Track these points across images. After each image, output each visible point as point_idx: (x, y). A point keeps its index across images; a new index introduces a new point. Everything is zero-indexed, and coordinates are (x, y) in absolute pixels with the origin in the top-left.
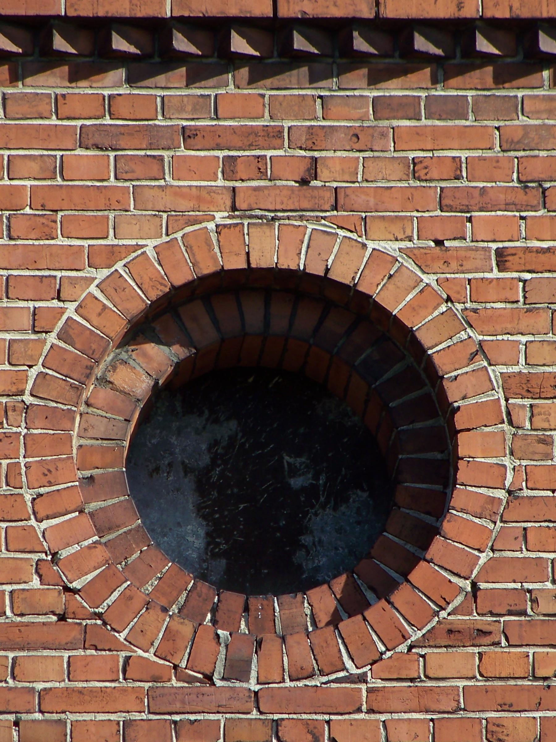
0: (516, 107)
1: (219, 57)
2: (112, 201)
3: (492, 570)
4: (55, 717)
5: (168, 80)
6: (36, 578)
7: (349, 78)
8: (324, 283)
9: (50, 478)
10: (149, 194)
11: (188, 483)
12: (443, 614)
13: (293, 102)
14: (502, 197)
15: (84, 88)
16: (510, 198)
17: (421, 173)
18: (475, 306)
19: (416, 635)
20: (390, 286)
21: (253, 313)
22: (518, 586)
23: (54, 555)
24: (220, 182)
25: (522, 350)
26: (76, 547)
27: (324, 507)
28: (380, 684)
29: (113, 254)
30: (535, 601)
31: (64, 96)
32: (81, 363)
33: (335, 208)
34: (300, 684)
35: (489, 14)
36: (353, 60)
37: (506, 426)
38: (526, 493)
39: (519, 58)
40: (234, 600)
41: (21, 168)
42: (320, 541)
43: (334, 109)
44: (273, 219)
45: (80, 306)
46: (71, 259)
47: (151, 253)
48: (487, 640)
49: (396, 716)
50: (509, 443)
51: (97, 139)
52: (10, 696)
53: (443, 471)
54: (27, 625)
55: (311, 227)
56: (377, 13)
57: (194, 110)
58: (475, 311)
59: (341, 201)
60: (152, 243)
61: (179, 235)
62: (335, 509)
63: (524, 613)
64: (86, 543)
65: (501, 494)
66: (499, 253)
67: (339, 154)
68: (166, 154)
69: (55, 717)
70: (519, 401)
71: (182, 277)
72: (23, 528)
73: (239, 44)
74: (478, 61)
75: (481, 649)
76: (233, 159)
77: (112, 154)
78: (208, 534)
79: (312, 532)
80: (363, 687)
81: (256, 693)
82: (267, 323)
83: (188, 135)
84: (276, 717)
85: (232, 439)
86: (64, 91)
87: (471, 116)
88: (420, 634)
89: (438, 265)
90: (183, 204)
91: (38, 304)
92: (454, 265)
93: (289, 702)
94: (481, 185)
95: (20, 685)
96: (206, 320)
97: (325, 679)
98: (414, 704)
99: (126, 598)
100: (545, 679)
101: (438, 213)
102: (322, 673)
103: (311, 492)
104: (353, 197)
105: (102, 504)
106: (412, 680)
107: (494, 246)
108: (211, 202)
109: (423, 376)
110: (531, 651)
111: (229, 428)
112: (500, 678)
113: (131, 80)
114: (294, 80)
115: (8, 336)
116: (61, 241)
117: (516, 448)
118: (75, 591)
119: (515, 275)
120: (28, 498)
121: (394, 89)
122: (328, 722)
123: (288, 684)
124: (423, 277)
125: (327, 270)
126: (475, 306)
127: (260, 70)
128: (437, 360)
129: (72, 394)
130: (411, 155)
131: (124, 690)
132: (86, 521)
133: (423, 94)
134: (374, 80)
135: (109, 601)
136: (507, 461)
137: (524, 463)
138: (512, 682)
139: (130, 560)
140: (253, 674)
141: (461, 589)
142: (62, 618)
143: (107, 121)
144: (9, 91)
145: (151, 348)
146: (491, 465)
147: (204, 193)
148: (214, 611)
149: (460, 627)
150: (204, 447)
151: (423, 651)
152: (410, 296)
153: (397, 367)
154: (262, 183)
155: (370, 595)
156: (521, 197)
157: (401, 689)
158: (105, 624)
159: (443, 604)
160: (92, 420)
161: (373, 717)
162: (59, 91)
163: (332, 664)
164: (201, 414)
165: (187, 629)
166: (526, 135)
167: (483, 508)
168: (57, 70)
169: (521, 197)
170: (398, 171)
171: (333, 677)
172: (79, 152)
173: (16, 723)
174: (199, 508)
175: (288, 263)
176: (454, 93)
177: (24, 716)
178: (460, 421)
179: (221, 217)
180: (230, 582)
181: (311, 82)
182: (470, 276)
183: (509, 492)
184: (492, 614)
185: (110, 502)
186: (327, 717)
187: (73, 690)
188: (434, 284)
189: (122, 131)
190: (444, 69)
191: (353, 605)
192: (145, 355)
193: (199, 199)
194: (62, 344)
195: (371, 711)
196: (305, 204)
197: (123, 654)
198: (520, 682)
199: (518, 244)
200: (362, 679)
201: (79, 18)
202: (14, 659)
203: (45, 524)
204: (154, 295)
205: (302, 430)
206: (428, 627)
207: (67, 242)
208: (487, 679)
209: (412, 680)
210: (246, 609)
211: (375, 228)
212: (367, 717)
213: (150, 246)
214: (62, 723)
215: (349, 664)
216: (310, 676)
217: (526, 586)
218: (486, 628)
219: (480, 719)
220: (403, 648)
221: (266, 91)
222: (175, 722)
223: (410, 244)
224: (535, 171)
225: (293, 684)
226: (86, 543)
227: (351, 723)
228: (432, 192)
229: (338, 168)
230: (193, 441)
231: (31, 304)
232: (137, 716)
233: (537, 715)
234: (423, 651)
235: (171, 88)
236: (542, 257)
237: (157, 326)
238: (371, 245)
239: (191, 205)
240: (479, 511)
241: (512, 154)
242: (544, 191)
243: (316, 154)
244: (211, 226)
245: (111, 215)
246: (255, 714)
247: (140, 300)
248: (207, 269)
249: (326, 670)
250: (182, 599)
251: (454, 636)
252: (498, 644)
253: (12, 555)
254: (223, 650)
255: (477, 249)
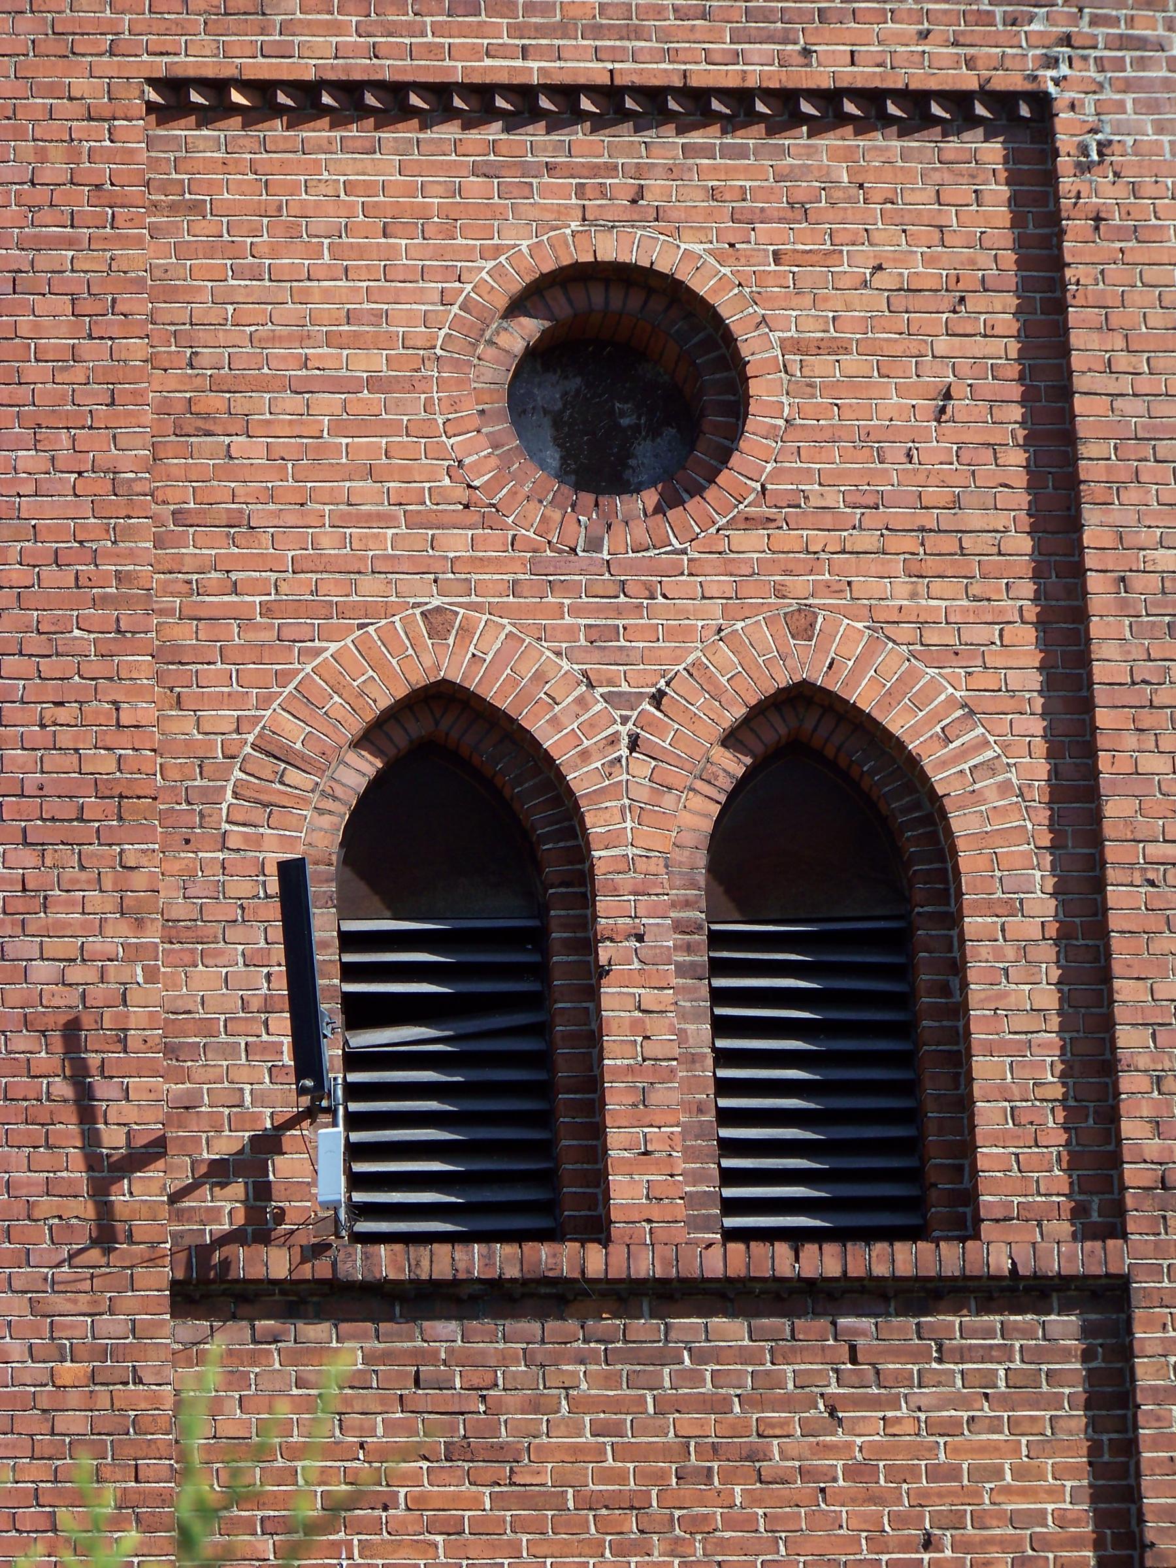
0: (787, 152)
1: (572, 113)
2: (496, 214)
3: (775, 475)
4: (463, 576)
5: (535, 129)
6: (447, 479)
7: (664, 130)
8: (650, 273)
9: (456, 407)
10: (522, 209)
11: (547, 422)
12: (741, 506)
13: (622, 146)
14: (776, 213)
15: (474, 135)
16: (782, 214)
17: (718, 197)
18: (758, 289)
19: (722, 522)
20: (698, 275)
21: (597, 296)
22: (795, 487)
23: (460, 462)
24: (574, 201)
25: (797, 321)
26: (476, 457)
27: (645, 439)
28: (697, 555)
29: (498, 250)
30: (806, 498)
31: (460, 140)
32: (476, 334)
33: (657, 220)
34: (639, 555)
35: (764, 85)
36: (667, 117)
37: (783, 374)
38: (798, 421)
39: (785, 117)
40: (587, 498)
41: (429, 190)
42: (643, 463)
43: (655, 151)
44: (613, 227)
45: (475, 286)
46: (468, 254)
47: (525, 250)
48: (773, 525)
49: (708, 578)
50: (785, 386)
51: (485, 170)
52: (431, 561)
53: (737, 408)
54: (441, 511)
55: (640, 233)
56: (685, 83)
57: (554, 150)
58: (759, 293)
59: (661, 214)
60: (525, 243)
61: (545, 238)
62: (653, 441)
63: (799, 506)
64: (482, 454)
65: (781, 422)
66: (775, 253)
67: (658, 182)
68: (534, 181)
69: (463, 576)
70: (792, 357)
71: (547, 267)
72: (437, 443)
73: (586, 104)
74: (756, 119)
75: (769, 532)
76: (584, 184)
77: (496, 181)
78: (561, 458)
79: (636, 458)
80: (685, 557)
81: (608, 561)
82: (607, 303)
83: (550, 168)
84: (623, 578)
85: (578, 391)
86: (461, 136)
87: (752, 157)
88: (725, 520)
89: (732, 261)
90: (548, 216)
91: (445, 285)
92: (743, 261)
93: (632, 567)
94: (761, 205)
95: (437, 554)
96: (563, 301)
97: (657, 552)
98: (722, 570)
99: (513, 493)
100: (815, 553)
101: (731, 224)
102: (655, 548)
103: (636, 428)
104: (669, 212)
105: (491, 429)
106: (720, 553)
107: (771, 248)
108: (568, 214)
109: (720, 341)
110: (805, 533)
111: (575, 383)
112: (783, 552)
113: (507, 129)
114: (625, 130)
115: (424, 307)
116: (460, 241)
117: (790, 390)
118: (476, 488)
119: (787, 268)
120: (440, 421)
121: (696, 138)
122: (660, 582)
123: (631, 555)
124: (722, 269)
125: (652, 264)
126: (758, 289)
127: (599, 123)
128: (732, 327)
129: (470, 348)
130: (710, 184)
131: (512, 558)
132: (482, 439)
133: (718, 142)
134: (680, 132)
135: (500, 495)
136: (784, 399)
137: (797, 400)
138: (792, 555)
139: (512, 469)
140: (606, 548)
141: (754, 489)
142: (467, 506)
143: (492, 157)
144: (421, 136)
145: (525, 320)
146: (773, 402)
147: (562, 209)
148: (573, 506)
149: (754, 516)
150: (558, 396)
151: (727, 533)
152: (712, 283)
153: (701, 336)
154: (604, 202)
155: (685, 496)
156: (790, 215)
157: (712, 560)
158: (498, 511)
159: (741, 499)
160: (482, 369)
161: (692, 578)
162: (457, 136)
163: (662, 541)
164: (555, 372)
165: (557, 515)
166: (791, 171)
167: (769, 433)
168: (455, 122)
169: (790, 215)
170: (701, 195)
171: (663, 550)
172: (472, 179)
173: (435, 581)
174: (555, 439)
175: (624, 258)
176: (740, 141)
177: (440, 576)
178: (750, 371)
179: (575, 225)
180: (578, 487)
181: (635, 132)
182: (755, 269)
183: (787, 421)
184: (776, 507)
185: (497, 428)
186: (659, 579)
187: (476, 558)
188: (729, 274)
189: (503, 165)
190: (730, 124)
191: (670, 501)
192: (520, 324)
193: (559, 212)
194: (462, 313)
195: (691, 574)
196: (636, 217)
197: (512, 532)
198: (797, 555)
199: (788, 247)
200: (684, 552)
201: (471, 84)
202: (433, 536)
203: (452, 440)
204: (528, 279)
205: (628, 385)
206: (731, 515)
207: (465, 242)
208: (774, 553)
209: (720, 553)
210: (597, 505)
211: (685, 235)
212: (688, 578)
213: (524, 245)
214: (468, 581)
215: (674, 541)
216: (647, 550)
217: (800, 487)
218: (771, 517)
219: (769, 581)
220: (713, 530)
221: (604, 137)
222: (550, 582)
223: (711, 246)
224: (799, 196)
225: (634, 555)
226: (482, 454)
227: (677, 583)
228: (725, 210)
229: (658, 191)
230: (550, 392)
231: (440, 285)
232: (522, 577)
233: (810, 578)
234: (727, 533)
235: (535, 134)
236: (806, 256)
237: (529, 305)
238: (683, 246)
239: (553, 217)
240: (765, 433)
241: (782, 184)
242: (806, 210)
243: (642, 182)
244: (568, 231)
245: (496, 224)
246: (607, 576)
247: (517, 284)
248: (566, 261)
249: (658, 545)
250: (550, 497)
251: (750, 522)
252: (780, 528)
253: (429, 461)
254: (583, 530)
255: (759, 250)
